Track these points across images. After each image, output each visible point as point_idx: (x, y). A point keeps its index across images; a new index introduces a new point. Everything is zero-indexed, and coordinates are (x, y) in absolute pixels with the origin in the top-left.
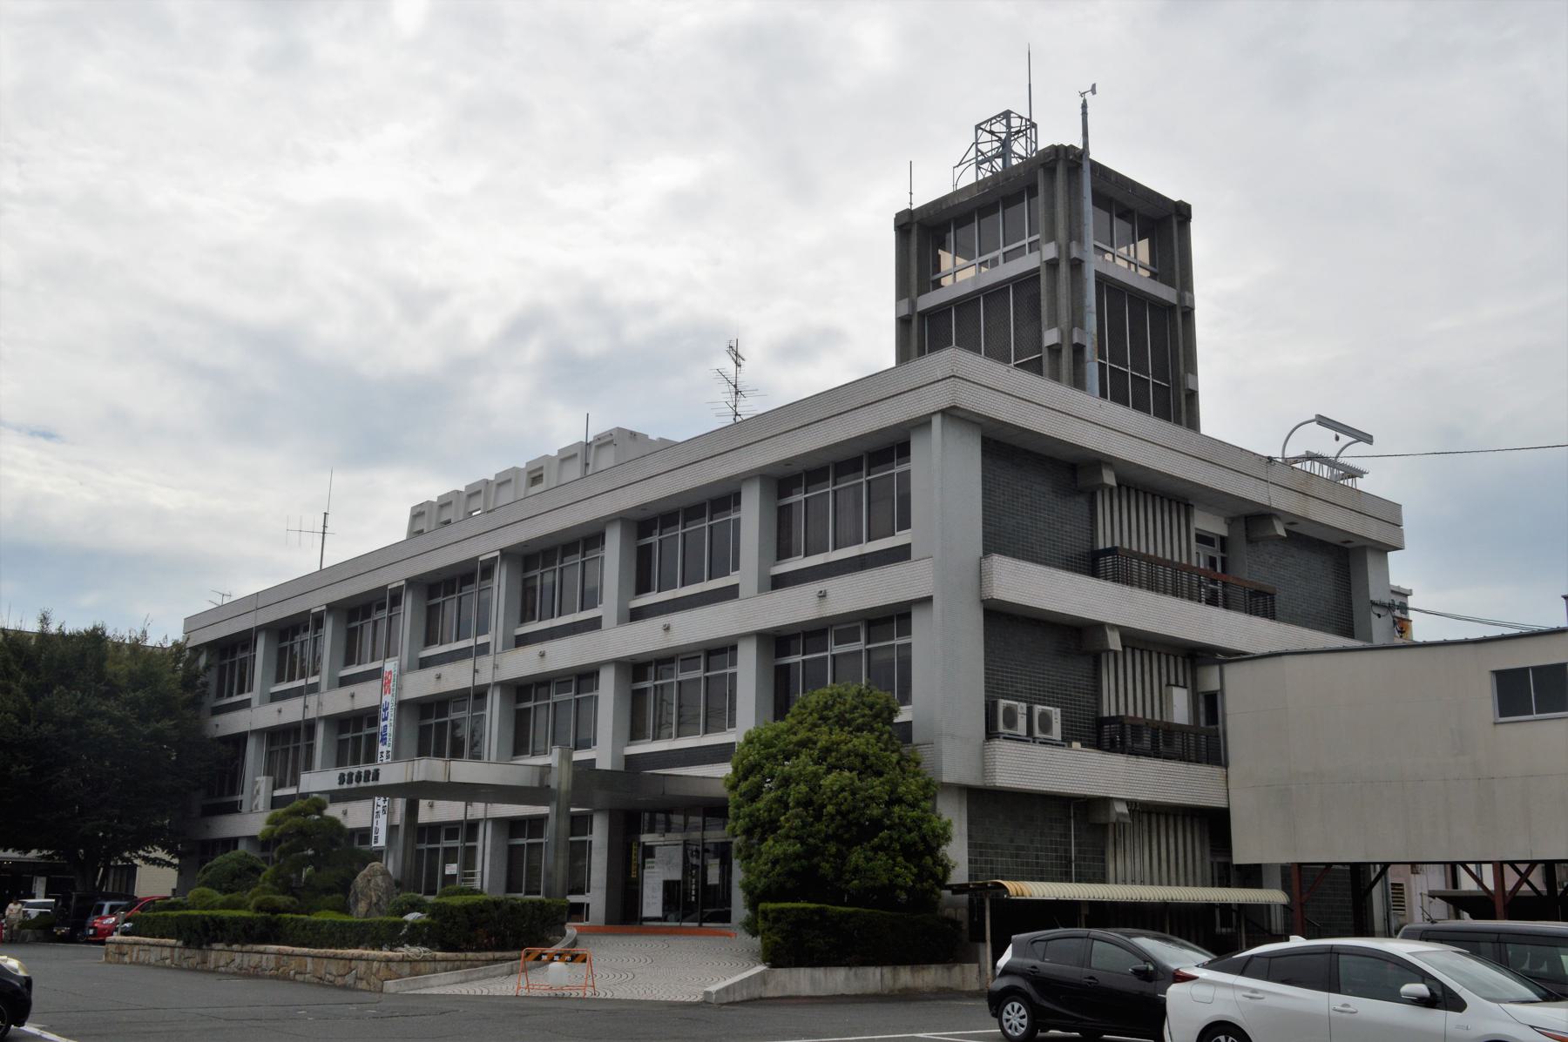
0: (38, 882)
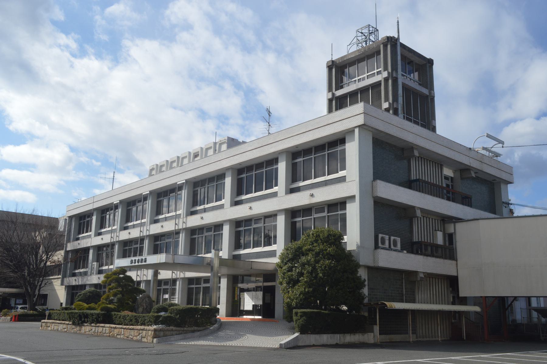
0: (12, 300)
